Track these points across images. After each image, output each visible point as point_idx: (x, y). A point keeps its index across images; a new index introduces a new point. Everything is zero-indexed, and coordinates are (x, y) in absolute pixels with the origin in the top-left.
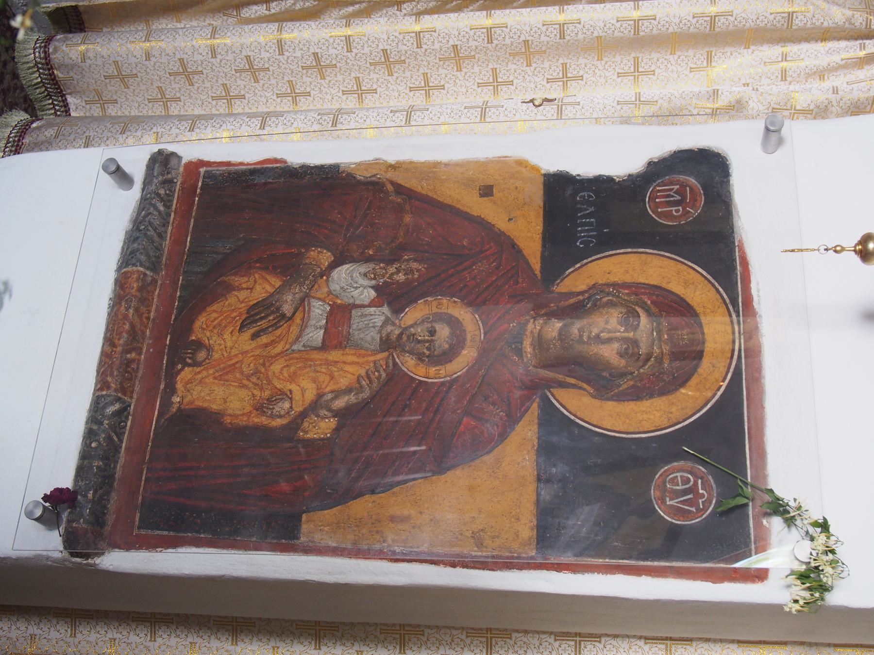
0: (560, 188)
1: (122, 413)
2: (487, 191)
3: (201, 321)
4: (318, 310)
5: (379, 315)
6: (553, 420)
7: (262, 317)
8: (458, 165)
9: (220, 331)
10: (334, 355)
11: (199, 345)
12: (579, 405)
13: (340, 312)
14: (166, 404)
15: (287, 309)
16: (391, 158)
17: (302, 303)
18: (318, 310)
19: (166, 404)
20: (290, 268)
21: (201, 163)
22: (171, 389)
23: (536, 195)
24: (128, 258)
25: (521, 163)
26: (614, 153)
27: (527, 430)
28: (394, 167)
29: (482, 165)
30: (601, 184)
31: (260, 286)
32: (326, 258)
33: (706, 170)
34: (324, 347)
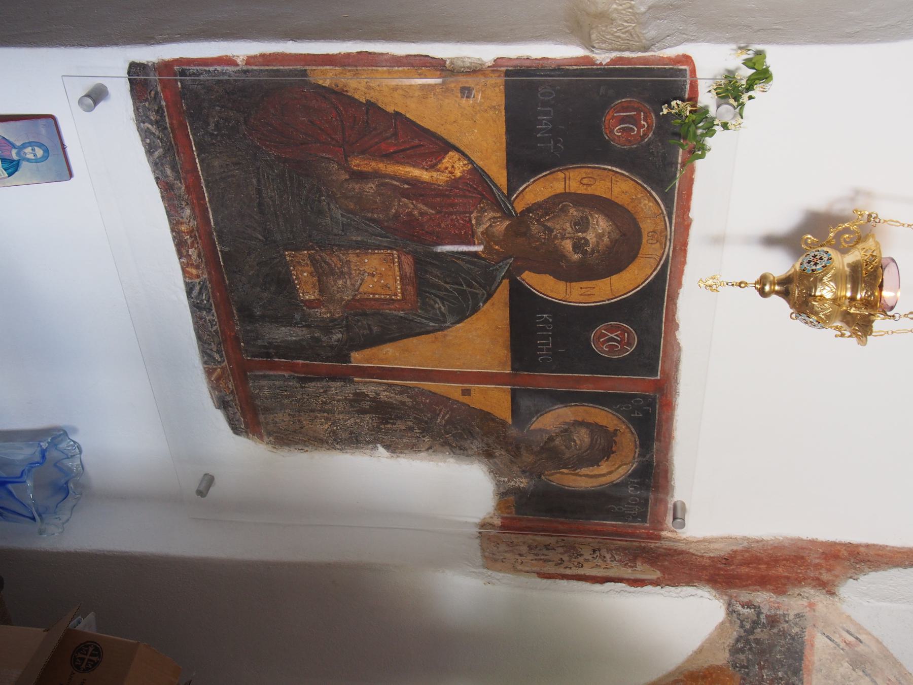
23: (492, 96)
27: (502, 293)
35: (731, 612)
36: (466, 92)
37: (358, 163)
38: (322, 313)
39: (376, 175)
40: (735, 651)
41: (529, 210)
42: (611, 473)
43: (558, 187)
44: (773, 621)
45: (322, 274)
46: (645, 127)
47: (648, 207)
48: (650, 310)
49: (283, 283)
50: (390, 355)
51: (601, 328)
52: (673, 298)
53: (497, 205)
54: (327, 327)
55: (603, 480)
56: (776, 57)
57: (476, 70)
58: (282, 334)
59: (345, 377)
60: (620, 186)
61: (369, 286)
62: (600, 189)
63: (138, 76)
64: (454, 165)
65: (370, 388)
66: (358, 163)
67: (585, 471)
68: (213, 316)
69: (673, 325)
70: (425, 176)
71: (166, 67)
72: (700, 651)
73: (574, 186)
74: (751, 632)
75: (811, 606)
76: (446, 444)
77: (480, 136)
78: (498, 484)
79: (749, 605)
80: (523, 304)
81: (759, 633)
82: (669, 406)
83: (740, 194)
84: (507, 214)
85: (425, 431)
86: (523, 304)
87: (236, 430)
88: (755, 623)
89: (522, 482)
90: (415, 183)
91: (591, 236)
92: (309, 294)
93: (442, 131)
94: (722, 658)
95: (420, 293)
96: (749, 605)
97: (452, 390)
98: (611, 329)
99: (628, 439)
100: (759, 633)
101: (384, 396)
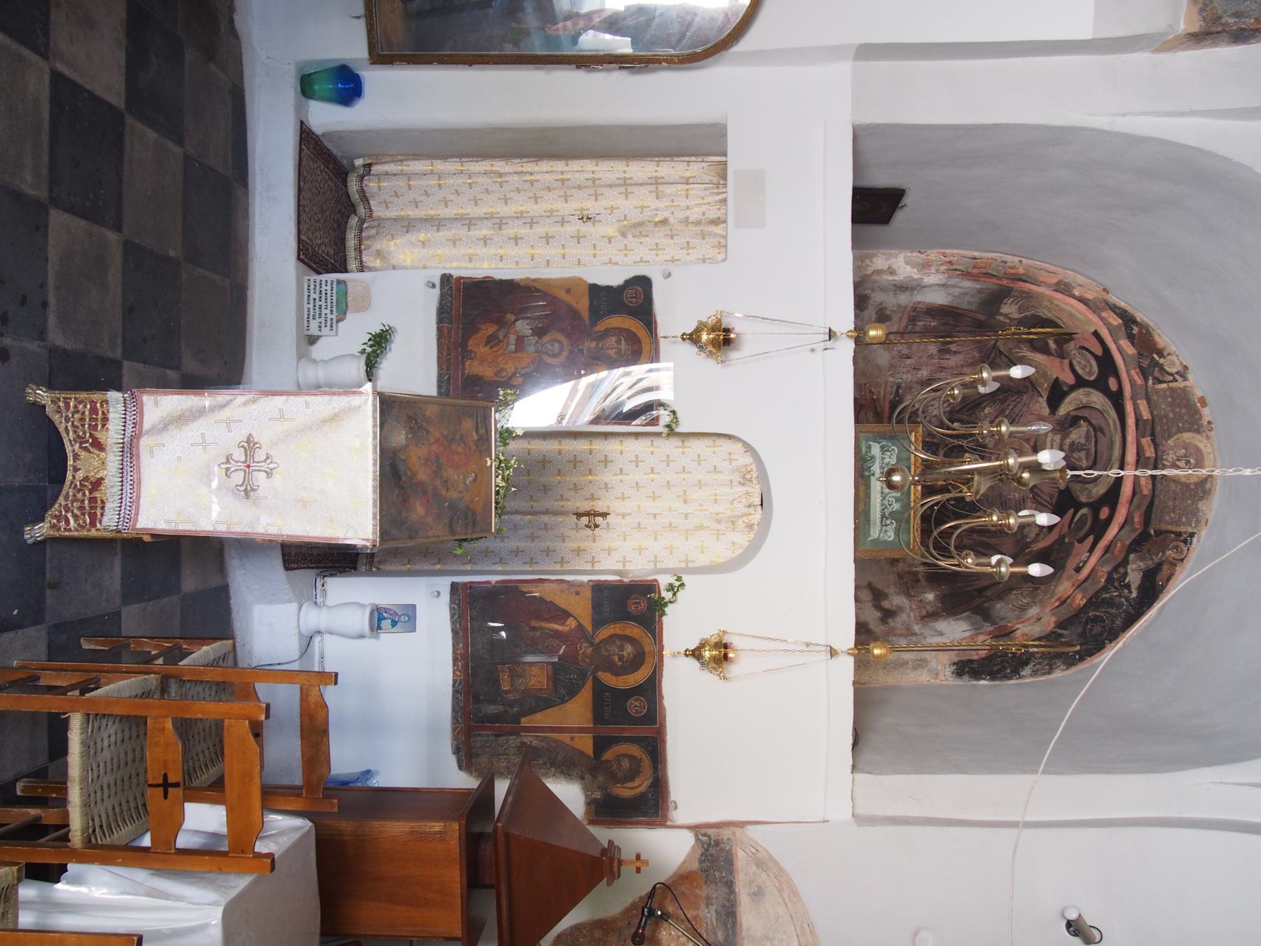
0: (594, 289)
1: (449, 379)
2: (568, 291)
3: (471, 342)
4: (512, 338)
5: (534, 339)
6: (596, 681)
7: (492, 341)
8: (560, 279)
9: (476, 344)
10: (519, 354)
11: (471, 352)
12: (607, 678)
13: (520, 340)
14: (463, 374)
15: (501, 337)
16: (533, 277)
17: (505, 336)
18: (512, 338)
19: (463, 374)
20: (501, 323)
21: (461, 278)
22: (464, 368)
23: (588, 594)
24: (440, 320)
25: (580, 279)
26: (613, 278)
27: (589, 684)
28: (535, 280)
29: (566, 280)
30: (609, 288)
31: (491, 329)
32: (513, 318)
33: (642, 284)
34: (516, 351)
35: (697, 839)
36: (577, 593)
37: (534, 623)
38: (511, 697)
39: (540, 628)
40: (701, 862)
41: (601, 642)
42: (641, 785)
43: (612, 632)
44: (717, 843)
45: (514, 675)
46: (643, 606)
47: (647, 641)
48: (651, 689)
49: (496, 682)
50: (539, 719)
51: (631, 700)
52: (660, 682)
53: (588, 641)
54: (511, 704)
55: (637, 791)
56: (685, 579)
57: (581, 584)
58: (492, 709)
59: (516, 733)
60: (634, 630)
61: (533, 682)
62: (628, 632)
63: (454, 587)
64: (572, 623)
65: (529, 739)
66: (534, 623)
67: (628, 785)
68: (461, 698)
69: (661, 697)
70: (559, 628)
71: (465, 584)
72: (684, 862)
73: (618, 631)
74: (707, 850)
75: (734, 833)
76: (562, 772)
77: (582, 610)
78: (587, 797)
79: (705, 835)
80: (600, 690)
81: (712, 851)
82: (663, 741)
83: (680, 628)
84: (592, 645)
85: (553, 764)
86: (600, 690)
87: (460, 768)
88: (709, 845)
89: (598, 795)
90: (556, 631)
91: (625, 654)
92: (505, 688)
93: (567, 609)
94: (695, 866)
95: (555, 685)
96: (705, 835)
97: (565, 737)
98: (637, 700)
99: (647, 763)
100: (712, 851)
101: (535, 743)
